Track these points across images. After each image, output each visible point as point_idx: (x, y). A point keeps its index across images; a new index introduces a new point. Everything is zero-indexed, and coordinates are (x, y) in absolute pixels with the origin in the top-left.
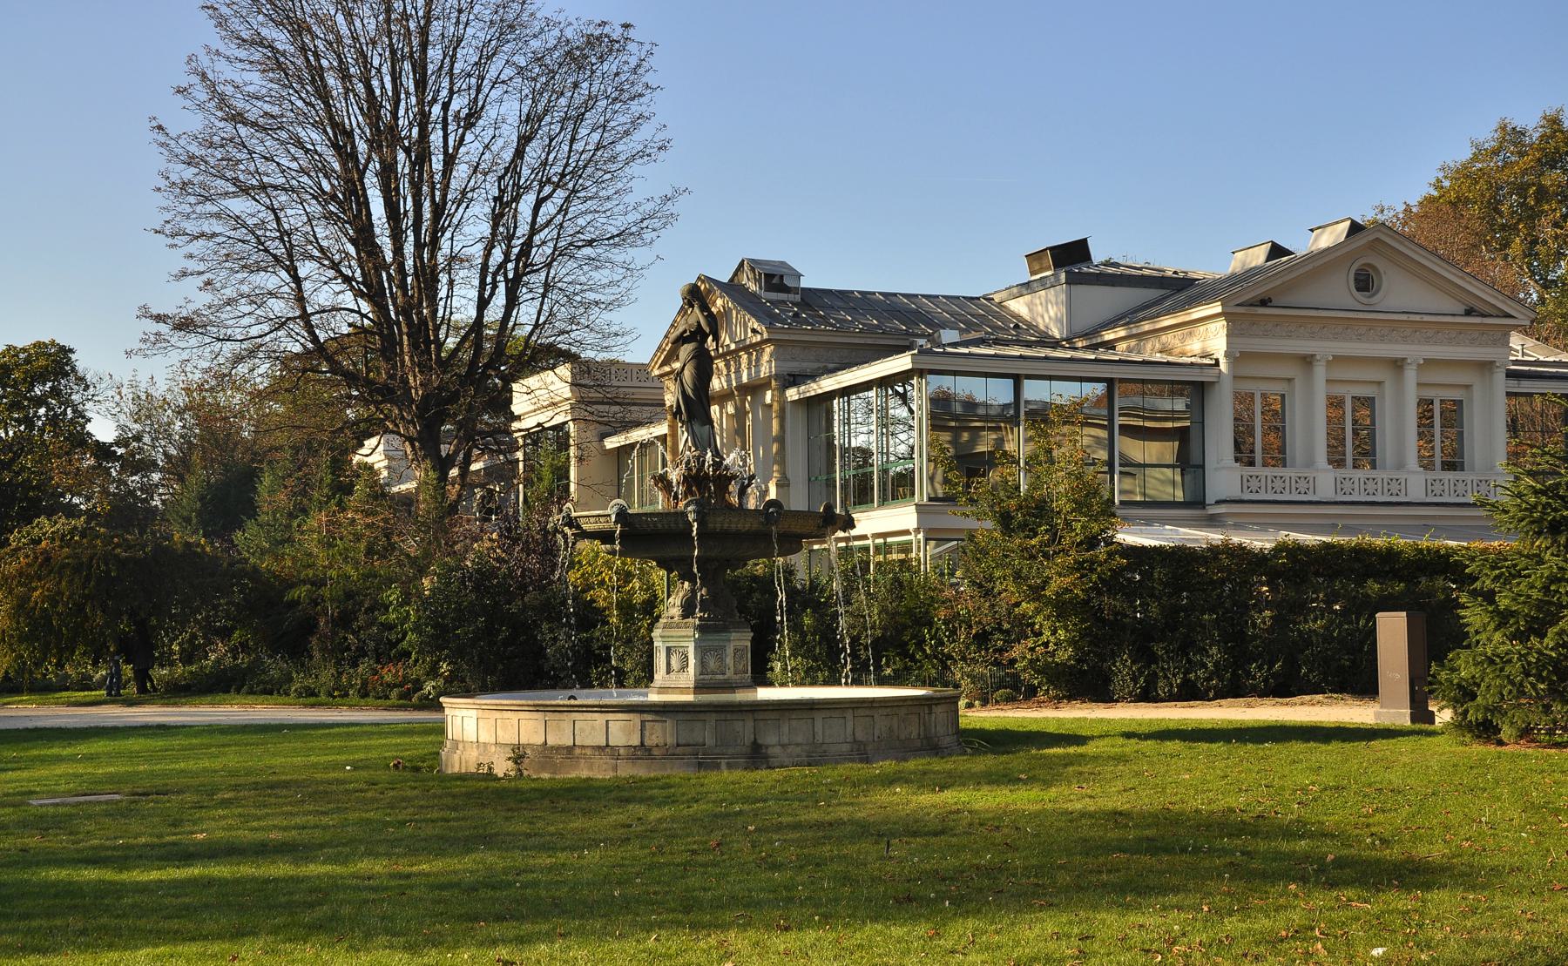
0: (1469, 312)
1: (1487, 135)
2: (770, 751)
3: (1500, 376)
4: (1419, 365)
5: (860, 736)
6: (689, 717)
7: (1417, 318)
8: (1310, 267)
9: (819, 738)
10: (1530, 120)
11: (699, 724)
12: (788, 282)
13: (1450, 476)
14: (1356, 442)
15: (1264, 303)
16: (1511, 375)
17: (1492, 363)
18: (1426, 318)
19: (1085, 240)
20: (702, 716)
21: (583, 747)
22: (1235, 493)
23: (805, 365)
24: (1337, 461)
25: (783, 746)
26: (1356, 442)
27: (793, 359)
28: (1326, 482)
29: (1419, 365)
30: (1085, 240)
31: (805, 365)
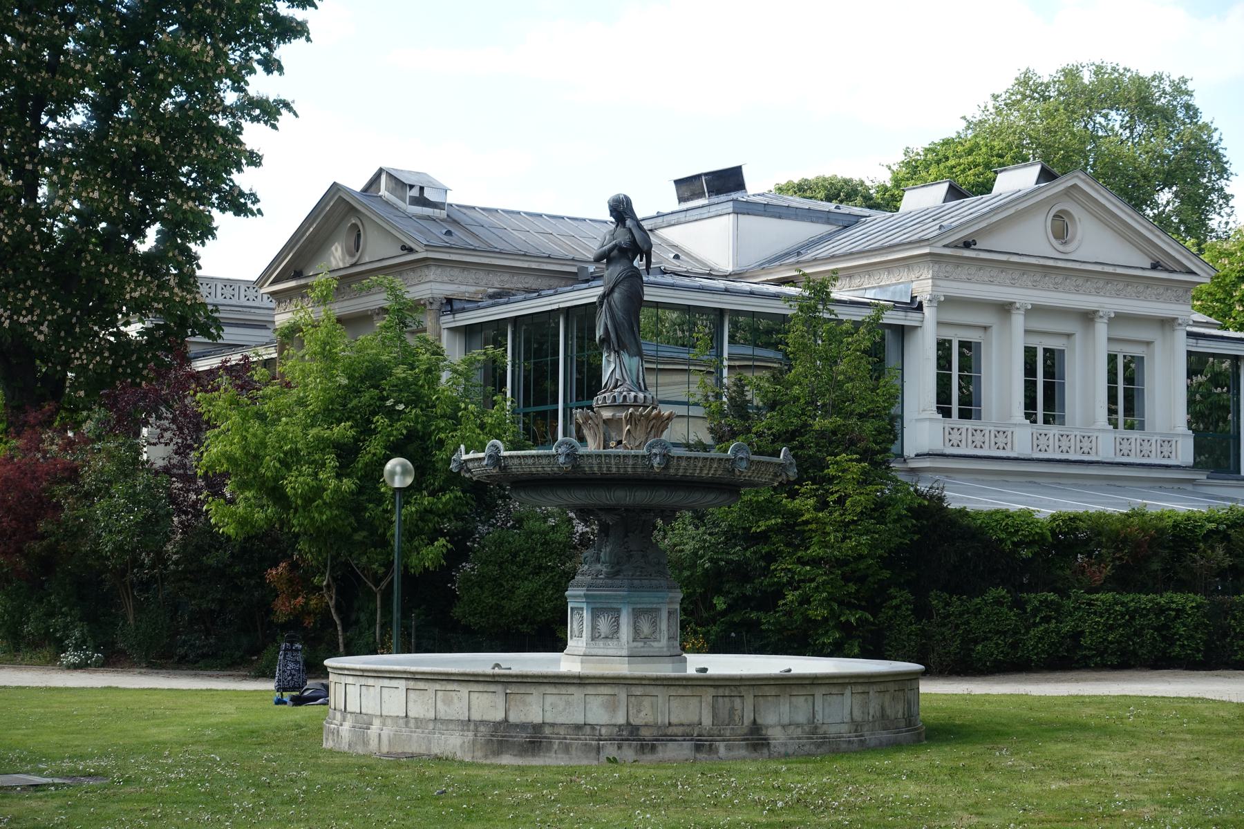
0: (1155, 267)
1: (1004, 83)
2: (770, 732)
3: (1180, 335)
4: (1110, 319)
5: (857, 715)
6: (681, 691)
7: (1111, 269)
8: (1012, 211)
9: (819, 717)
10: (1047, 70)
11: (695, 701)
12: (429, 194)
13: (967, 424)
14: (1045, 392)
15: (967, 245)
16: (1190, 335)
17: (1174, 319)
18: (1119, 271)
19: (740, 168)
20: (698, 691)
21: (553, 725)
22: (938, 446)
23: (463, 288)
24: (1030, 416)
25: (784, 727)
26: (1045, 392)
27: (452, 282)
28: (1024, 438)
29: (1110, 319)
30: (740, 168)
31: (463, 288)
